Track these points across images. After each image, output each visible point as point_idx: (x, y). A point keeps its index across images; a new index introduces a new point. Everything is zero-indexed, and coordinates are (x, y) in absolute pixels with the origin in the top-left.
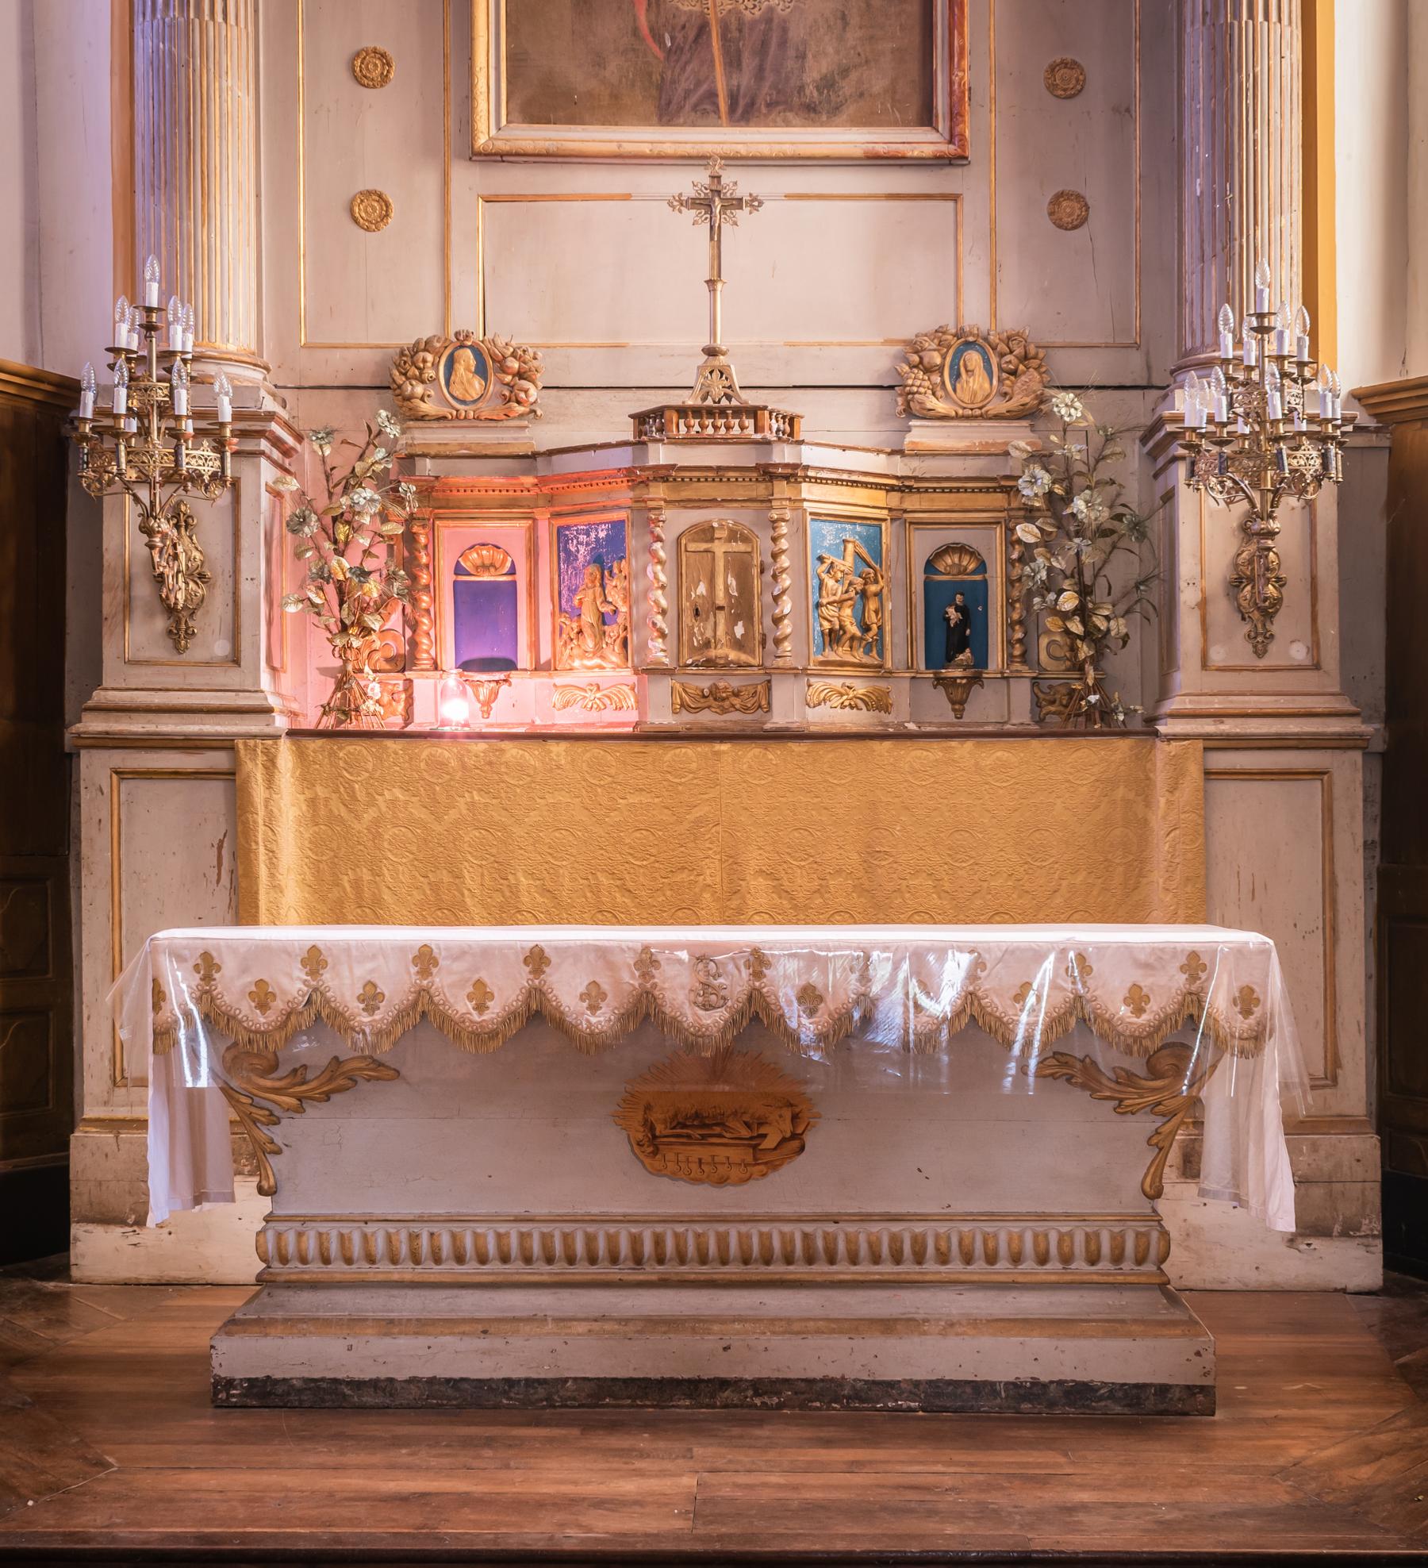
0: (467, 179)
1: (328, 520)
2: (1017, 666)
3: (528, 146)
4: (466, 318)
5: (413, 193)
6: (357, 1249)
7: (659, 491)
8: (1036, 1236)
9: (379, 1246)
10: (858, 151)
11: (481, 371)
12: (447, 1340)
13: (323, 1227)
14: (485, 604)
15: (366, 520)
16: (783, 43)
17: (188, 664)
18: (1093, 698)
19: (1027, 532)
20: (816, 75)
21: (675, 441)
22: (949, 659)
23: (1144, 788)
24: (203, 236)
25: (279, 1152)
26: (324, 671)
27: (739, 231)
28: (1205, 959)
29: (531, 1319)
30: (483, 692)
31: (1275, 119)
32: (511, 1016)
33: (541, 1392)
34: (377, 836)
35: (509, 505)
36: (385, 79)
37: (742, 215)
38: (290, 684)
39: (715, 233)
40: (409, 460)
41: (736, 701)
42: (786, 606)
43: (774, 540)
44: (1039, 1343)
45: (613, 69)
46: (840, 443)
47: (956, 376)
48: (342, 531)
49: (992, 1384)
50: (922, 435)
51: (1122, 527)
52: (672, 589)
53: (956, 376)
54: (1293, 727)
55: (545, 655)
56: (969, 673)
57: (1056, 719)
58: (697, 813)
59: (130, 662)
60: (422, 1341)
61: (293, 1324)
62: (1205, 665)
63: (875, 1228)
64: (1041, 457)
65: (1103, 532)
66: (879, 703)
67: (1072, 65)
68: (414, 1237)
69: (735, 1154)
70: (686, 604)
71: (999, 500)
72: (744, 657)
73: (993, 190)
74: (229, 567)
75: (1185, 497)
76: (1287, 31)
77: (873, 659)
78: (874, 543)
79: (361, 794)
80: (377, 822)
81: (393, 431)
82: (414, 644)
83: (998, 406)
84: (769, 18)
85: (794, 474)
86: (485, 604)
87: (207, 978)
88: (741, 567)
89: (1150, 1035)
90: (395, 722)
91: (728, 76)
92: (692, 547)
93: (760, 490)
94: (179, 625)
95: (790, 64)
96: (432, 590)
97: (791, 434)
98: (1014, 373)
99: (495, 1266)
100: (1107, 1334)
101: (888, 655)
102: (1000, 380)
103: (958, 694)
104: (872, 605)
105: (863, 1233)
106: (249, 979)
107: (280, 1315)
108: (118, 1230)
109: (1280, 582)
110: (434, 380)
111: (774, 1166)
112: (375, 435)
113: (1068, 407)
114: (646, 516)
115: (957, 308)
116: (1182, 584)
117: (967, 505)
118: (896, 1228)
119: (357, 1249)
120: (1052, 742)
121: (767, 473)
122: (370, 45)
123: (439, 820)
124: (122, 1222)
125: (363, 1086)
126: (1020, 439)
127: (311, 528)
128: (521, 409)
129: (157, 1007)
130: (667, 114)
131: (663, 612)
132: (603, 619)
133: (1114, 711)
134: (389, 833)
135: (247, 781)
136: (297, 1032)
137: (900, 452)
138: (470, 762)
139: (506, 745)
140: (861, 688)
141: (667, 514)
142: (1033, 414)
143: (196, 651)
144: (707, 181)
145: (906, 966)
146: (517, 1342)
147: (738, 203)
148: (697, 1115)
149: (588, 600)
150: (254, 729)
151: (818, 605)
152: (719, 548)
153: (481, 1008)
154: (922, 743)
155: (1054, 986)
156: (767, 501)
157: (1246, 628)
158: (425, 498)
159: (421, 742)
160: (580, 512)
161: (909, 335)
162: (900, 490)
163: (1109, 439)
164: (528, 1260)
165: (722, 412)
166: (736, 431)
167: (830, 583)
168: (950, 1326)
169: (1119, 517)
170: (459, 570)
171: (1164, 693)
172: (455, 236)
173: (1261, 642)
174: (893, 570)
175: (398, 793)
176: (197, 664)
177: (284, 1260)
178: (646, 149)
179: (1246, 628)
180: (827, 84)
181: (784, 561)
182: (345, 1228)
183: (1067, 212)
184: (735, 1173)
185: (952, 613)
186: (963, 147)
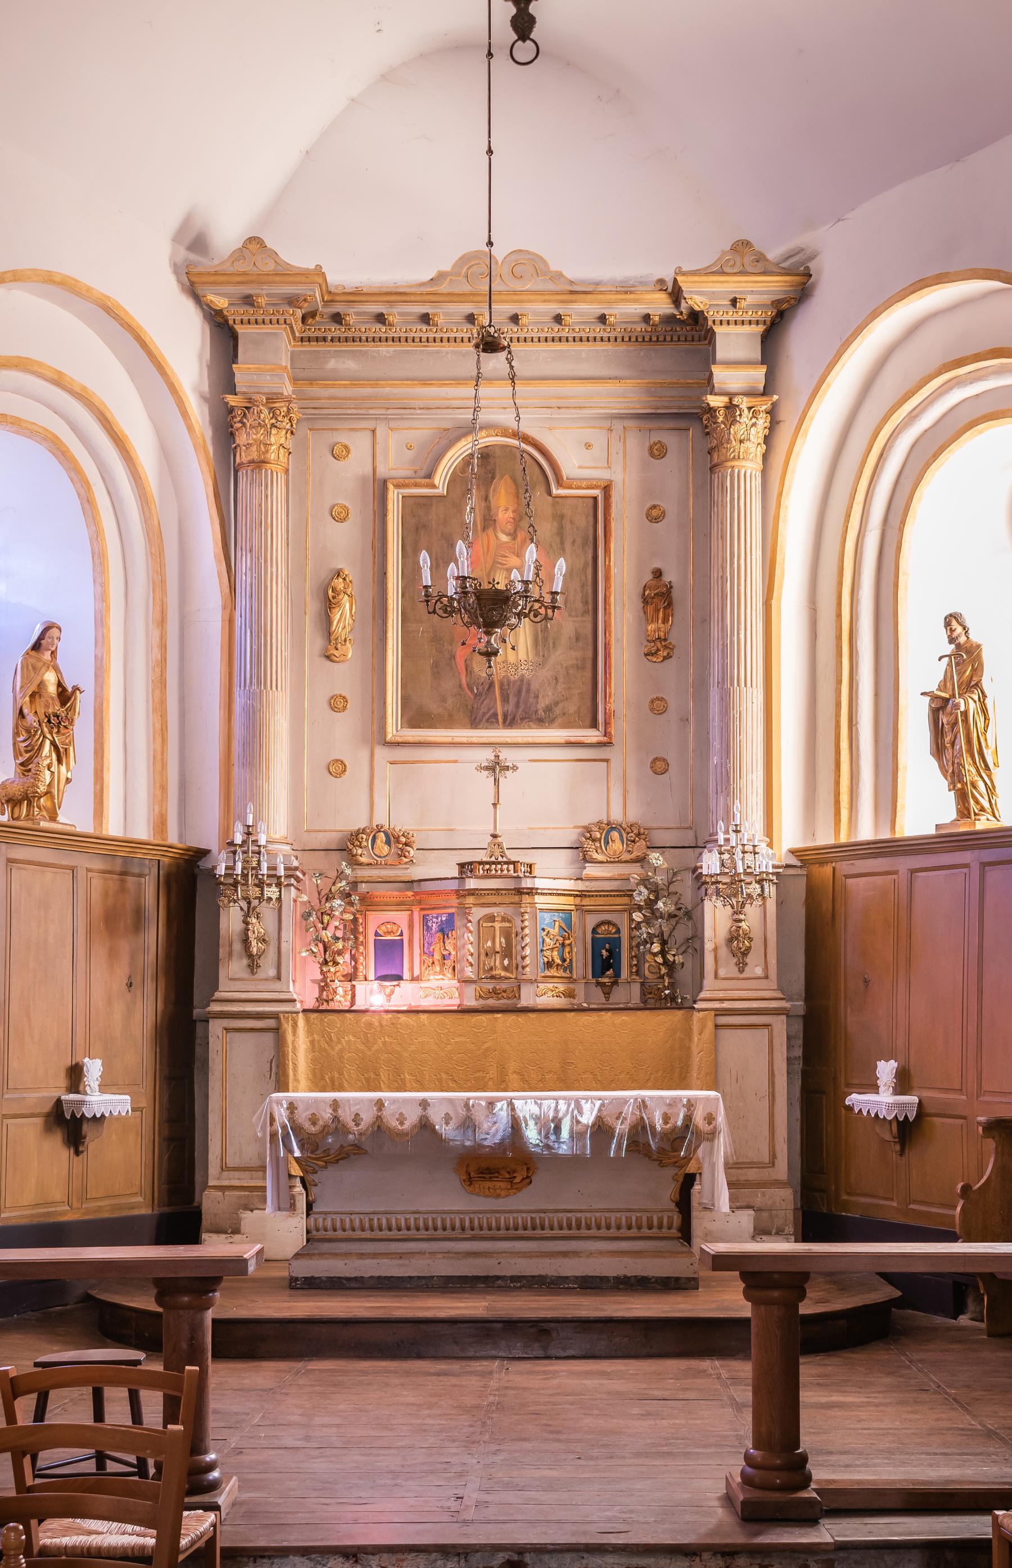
0: (382, 754)
1: (319, 914)
2: (634, 977)
3: (411, 739)
4: (381, 818)
5: (357, 760)
6: (348, 1225)
7: (470, 900)
8: (627, 1218)
9: (357, 1223)
10: (562, 741)
11: (388, 842)
12: (386, 1260)
13: (334, 1216)
14: (389, 951)
15: (337, 913)
16: (528, 691)
17: (257, 980)
18: (667, 992)
19: (637, 916)
20: (543, 705)
21: (477, 877)
22: (603, 974)
23: (688, 1032)
24: (265, 787)
25: (316, 1185)
26: (313, 981)
27: (507, 780)
28: (693, 1102)
29: (419, 1253)
30: (388, 991)
31: (749, 731)
32: (414, 1127)
33: (423, 1282)
34: (341, 1057)
35: (400, 905)
36: (345, 708)
37: (509, 773)
38: (301, 989)
39: (496, 781)
40: (354, 884)
41: (504, 994)
42: (528, 951)
43: (522, 921)
44: (627, 1260)
45: (450, 702)
46: (553, 877)
47: (607, 843)
48: (326, 918)
49: (607, 1277)
50: (591, 870)
51: (680, 913)
52: (476, 944)
53: (607, 843)
54: (755, 1005)
55: (416, 973)
56: (612, 980)
57: (652, 1001)
58: (486, 1045)
59: (231, 979)
60: (375, 1261)
61: (322, 1255)
62: (716, 976)
63: (560, 1215)
64: (644, 881)
65: (671, 916)
66: (570, 994)
67: (662, 699)
68: (371, 1220)
69: (503, 1185)
70: (482, 951)
71: (625, 900)
72: (508, 975)
73: (624, 757)
74: (276, 936)
75: (708, 905)
76: (755, 691)
77: (567, 974)
78: (568, 921)
79: (334, 1039)
80: (341, 1051)
81: (348, 871)
82: (356, 968)
83: (626, 857)
84: (522, 679)
85: (532, 892)
86: (389, 951)
87: (292, 1113)
88: (507, 934)
89: (671, 1133)
90: (346, 1005)
91: (503, 706)
92: (485, 925)
93: (516, 898)
94: (253, 963)
95: (531, 700)
96: (364, 944)
97: (530, 873)
98: (633, 841)
99: (404, 1232)
100: (655, 1257)
101: (574, 973)
102: (627, 845)
103: (607, 990)
104: (567, 950)
105: (556, 1217)
106: (309, 1112)
107: (316, 1252)
108: (224, 1236)
109: (750, 939)
110: (366, 847)
111: (519, 1190)
112: (340, 875)
113: (656, 858)
114: (464, 911)
115: (608, 811)
116: (706, 941)
117: (611, 903)
118: (569, 1215)
119: (348, 1225)
120: (647, 1012)
121: (519, 891)
122: (338, 693)
123: (369, 1049)
124: (226, 1232)
125: (353, 1157)
126: (635, 872)
127: (313, 918)
128: (406, 860)
129: (271, 1124)
130: (474, 723)
131: (472, 955)
132: (444, 957)
133: (676, 998)
134: (346, 1055)
135: (284, 1032)
136: (328, 1134)
137: (581, 879)
138: (384, 1023)
139: (400, 1015)
140: (561, 988)
141: (474, 910)
142: (642, 860)
143: (261, 974)
144: (493, 758)
145: (573, 1106)
146: (414, 1261)
147: (507, 768)
148: (488, 1169)
149: (437, 949)
150: (288, 1009)
151: (542, 951)
152: (497, 925)
153: (402, 1123)
154: (589, 1013)
155: (632, 1113)
156: (519, 904)
157: (735, 960)
158: (362, 900)
159: (361, 1014)
160: (434, 908)
161: (586, 824)
162: (580, 896)
163: (675, 874)
164: (418, 1229)
165: (499, 863)
166: (505, 872)
167: (548, 940)
168: (590, 1254)
169: (679, 909)
170: (377, 934)
171: (701, 989)
172: (376, 780)
173: (742, 966)
174: (577, 932)
175: (351, 1038)
176: (261, 980)
177: (318, 1230)
178: (465, 740)
179: (735, 960)
180: (548, 709)
181: (527, 931)
182: (343, 1217)
183: (659, 766)
184: (503, 1193)
185: (604, 952)
186: (610, 738)
